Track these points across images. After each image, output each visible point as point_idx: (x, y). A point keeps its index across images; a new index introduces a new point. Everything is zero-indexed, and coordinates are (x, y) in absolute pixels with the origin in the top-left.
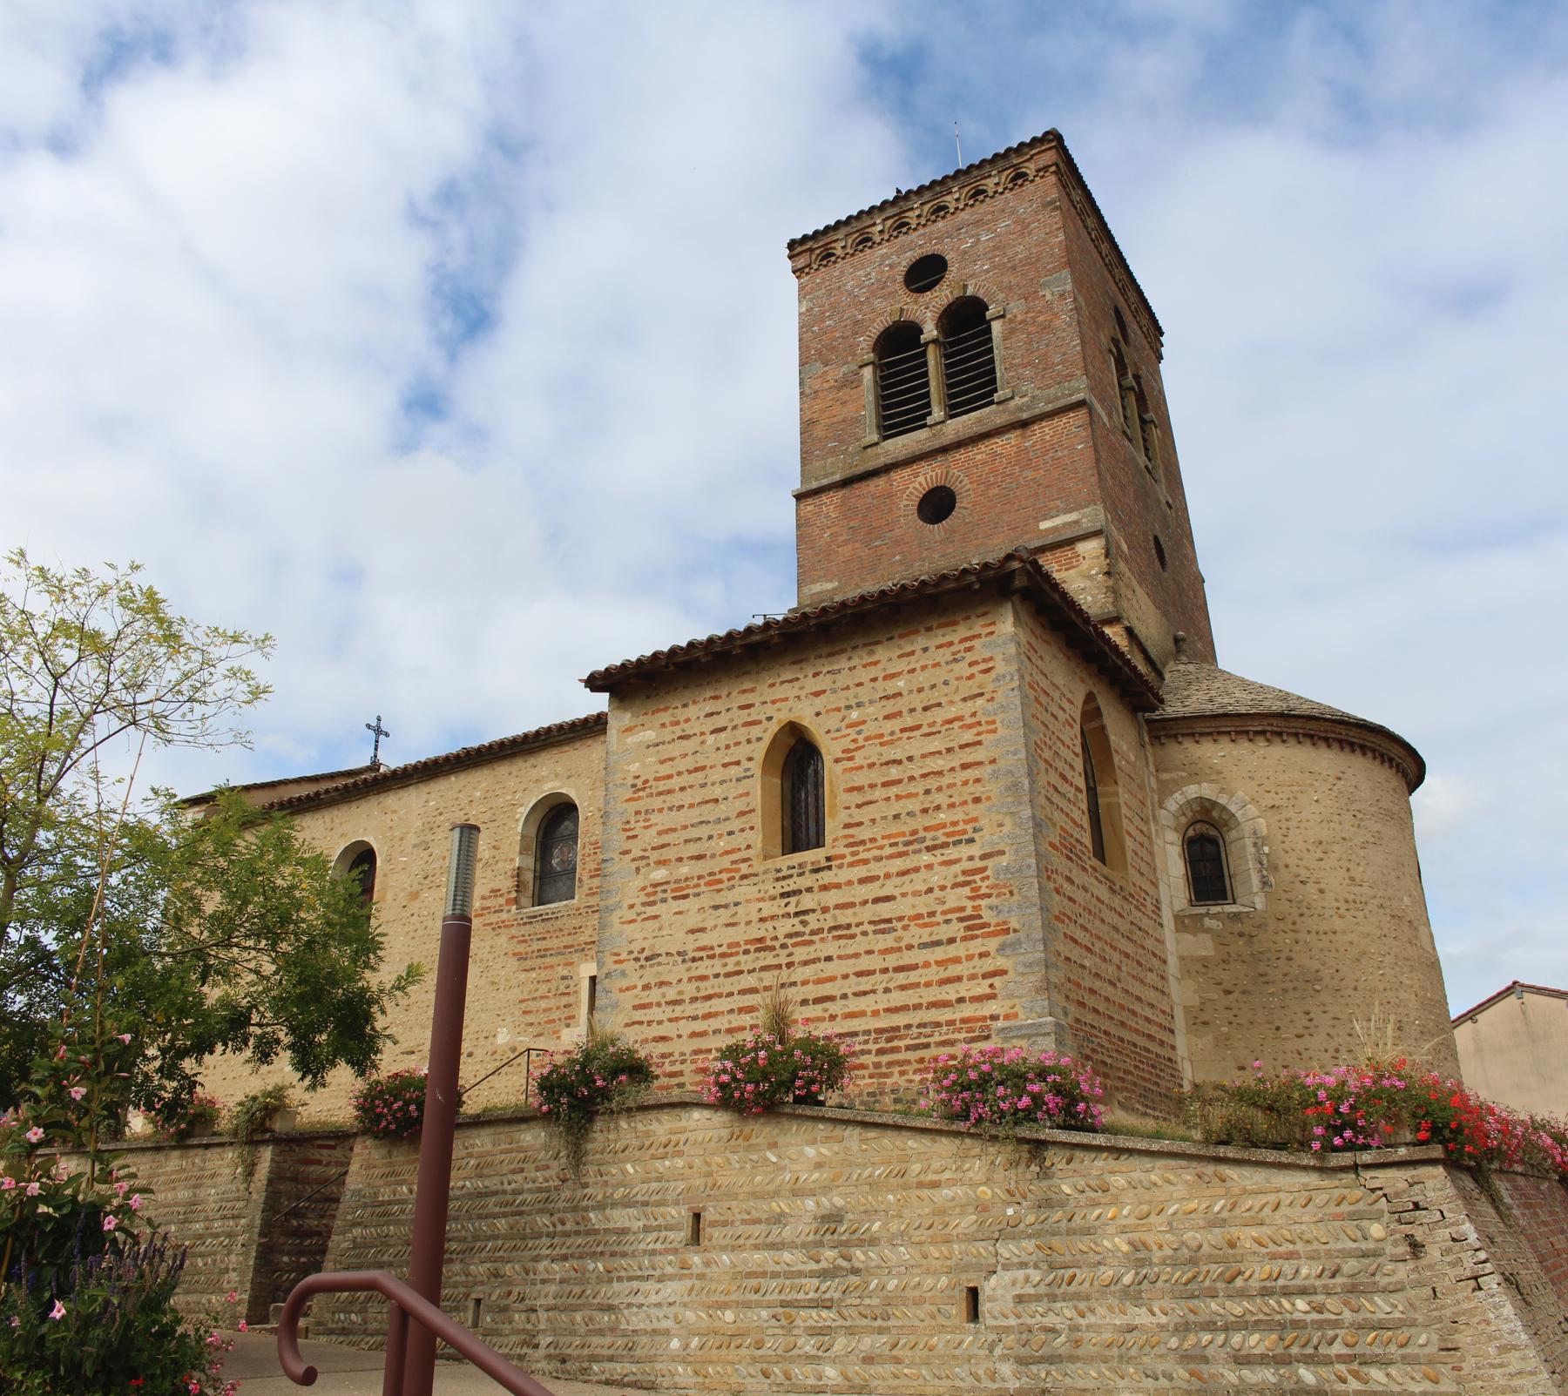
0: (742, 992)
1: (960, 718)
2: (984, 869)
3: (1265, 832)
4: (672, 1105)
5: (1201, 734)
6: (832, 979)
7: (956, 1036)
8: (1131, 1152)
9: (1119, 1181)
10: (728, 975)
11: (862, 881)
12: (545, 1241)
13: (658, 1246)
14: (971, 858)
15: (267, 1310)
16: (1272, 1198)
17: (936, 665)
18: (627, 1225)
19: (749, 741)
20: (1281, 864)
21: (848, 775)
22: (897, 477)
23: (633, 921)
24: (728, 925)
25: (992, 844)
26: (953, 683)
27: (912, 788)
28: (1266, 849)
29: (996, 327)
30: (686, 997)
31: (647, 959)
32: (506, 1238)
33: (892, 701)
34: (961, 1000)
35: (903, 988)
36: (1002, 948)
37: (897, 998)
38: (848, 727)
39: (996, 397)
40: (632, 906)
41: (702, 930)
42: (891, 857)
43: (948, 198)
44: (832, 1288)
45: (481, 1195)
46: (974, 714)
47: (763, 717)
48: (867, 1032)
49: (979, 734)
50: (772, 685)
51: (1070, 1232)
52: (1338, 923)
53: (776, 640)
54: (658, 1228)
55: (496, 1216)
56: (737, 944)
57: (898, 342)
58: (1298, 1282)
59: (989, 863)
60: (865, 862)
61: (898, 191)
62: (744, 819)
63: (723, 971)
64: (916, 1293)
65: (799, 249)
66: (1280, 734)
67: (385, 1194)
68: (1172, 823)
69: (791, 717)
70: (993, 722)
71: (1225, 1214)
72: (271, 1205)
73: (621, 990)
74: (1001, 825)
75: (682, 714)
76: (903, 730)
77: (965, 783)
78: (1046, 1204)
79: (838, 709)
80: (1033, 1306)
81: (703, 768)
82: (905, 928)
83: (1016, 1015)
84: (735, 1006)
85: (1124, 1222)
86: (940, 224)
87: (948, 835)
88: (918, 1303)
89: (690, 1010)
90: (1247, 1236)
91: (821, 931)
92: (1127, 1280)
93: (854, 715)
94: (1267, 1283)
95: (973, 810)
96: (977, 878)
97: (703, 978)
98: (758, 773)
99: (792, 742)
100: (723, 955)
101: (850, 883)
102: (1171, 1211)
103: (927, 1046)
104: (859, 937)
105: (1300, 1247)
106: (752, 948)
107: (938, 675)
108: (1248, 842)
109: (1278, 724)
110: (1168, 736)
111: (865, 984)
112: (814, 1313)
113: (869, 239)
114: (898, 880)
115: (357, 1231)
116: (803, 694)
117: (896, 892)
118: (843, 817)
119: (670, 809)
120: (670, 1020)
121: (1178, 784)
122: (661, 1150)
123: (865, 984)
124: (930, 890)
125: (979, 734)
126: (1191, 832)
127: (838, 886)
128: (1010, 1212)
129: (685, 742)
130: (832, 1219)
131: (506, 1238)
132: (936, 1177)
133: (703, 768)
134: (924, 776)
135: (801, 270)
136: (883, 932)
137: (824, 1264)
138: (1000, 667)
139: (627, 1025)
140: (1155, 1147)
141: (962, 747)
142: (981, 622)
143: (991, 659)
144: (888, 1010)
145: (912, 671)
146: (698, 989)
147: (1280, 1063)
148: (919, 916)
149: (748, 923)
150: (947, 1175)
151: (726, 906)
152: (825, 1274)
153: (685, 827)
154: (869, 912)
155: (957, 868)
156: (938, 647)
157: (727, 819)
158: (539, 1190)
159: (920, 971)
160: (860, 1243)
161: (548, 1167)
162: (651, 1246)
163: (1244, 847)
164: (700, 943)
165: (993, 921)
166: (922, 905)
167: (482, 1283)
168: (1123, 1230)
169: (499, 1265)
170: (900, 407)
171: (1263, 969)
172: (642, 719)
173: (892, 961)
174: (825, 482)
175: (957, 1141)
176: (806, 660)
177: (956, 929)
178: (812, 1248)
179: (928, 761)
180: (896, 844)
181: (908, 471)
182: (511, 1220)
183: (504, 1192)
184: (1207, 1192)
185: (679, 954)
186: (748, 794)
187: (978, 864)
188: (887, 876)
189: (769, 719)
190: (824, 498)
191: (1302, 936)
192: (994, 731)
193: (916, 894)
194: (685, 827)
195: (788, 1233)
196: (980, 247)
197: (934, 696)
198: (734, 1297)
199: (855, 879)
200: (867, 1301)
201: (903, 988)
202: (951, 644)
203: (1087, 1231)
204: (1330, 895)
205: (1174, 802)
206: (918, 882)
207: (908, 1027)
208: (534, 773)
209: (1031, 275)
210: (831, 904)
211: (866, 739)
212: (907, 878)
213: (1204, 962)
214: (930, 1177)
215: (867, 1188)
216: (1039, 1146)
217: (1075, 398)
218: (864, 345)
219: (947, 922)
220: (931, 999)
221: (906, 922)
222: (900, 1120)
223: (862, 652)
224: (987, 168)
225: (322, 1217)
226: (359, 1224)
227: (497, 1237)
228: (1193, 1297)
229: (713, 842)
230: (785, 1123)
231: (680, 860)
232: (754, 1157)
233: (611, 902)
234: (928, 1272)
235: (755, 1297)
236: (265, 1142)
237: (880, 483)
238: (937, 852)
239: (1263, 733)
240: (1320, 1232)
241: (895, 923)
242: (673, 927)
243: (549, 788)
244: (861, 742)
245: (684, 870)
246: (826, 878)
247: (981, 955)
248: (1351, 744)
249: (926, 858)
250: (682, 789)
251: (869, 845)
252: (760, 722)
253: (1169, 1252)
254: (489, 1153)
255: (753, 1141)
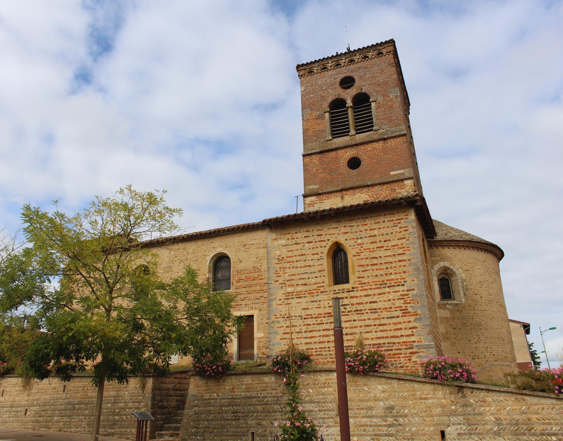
0: (324, 330)
1: (397, 245)
2: (408, 295)
3: (464, 278)
4: (326, 371)
5: (445, 246)
6: (356, 327)
7: (401, 347)
8: (493, 391)
9: (489, 399)
10: (318, 324)
11: (365, 296)
12: (278, 413)
13: (325, 416)
14: (403, 291)
15: (155, 434)
16: (541, 406)
17: (388, 227)
18: (312, 409)
19: (321, 247)
20: (469, 288)
21: (358, 261)
22: (340, 152)
23: (281, 304)
24: (317, 308)
25: (410, 286)
26: (394, 234)
27: (381, 267)
28: (465, 284)
29: (373, 105)
30: (303, 331)
31: (287, 317)
32: (262, 412)
33: (373, 238)
34: (402, 336)
35: (382, 331)
36: (415, 320)
37: (380, 334)
38: (357, 245)
39: (374, 128)
40: (280, 300)
41: (308, 309)
42: (375, 289)
43: (355, 57)
44: (392, 430)
45: (249, 398)
46: (402, 244)
47: (326, 239)
48: (370, 345)
49: (404, 251)
50: (329, 229)
51: (474, 414)
52: (486, 308)
53: (333, 215)
54: (325, 410)
55: (256, 405)
56: (321, 314)
57: (337, 105)
58: (552, 432)
59: (410, 293)
60: (366, 290)
61: (337, 53)
62: (321, 273)
63: (316, 323)
64: (423, 432)
65: (301, 68)
66: (468, 247)
67: (207, 396)
68: (435, 274)
69: (337, 240)
70: (409, 247)
71: (526, 411)
72: (153, 399)
73: (278, 328)
74: (413, 281)
75: (295, 236)
76: (377, 248)
77: (400, 266)
78: (465, 405)
79: (354, 239)
80: (464, 437)
81: (304, 255)
82: (381, 312)
83: (421, 341)
84: (321, 334)
85: (492, 412)
86: (352, 66)
87: (395, 283)
88: (424, 435)
89: (305, 335)
90: (534, 417)
91: (351, 311)
92: (495, 429)
93: (360, 241)
94: (543, 432)
95: (403, 275)
96: (406, 297)
97: (309, 325)
98: (325, 258)
99: (335, 248)
100: (316, 318)
101: (361, 296)
102: (508, 409)
103: (392, 350)
104: (365, 314)
105: (552, 421)
106: (327, 316)
107: (389, 230)
108: (460, 281)
109: (468, 243)
110: (434, 246)
111: (368, 329)
112: (387, 438)
113: (326, 68)
114: (378, 296)
115: (196, 409)
116: (340, 232)
117: (378, 300)
118: (357, 274)
119: (293, 268)
120: (297, 338)
121: (438, 262)
122: (323, 385)
123: (368, 329)
124: (390, 300)
125: (404, 251)
126: (440, 277)
127: (357, 297)
128: (453, 407)
129: (297, 245)
130: (391, 408)
131: (262, 412)
132: (426, 396)
133: (304, 255)
134: (386, 263)
135: (302, 76)
136: (373, 313)
137: (388, 423)
138: (410, 230)
139: (281, 339)
140: (502, 390)
141: (398, 255)
142: (403, 214)
143: (407, 227)
144: (376, 338)
145: (380, 228)
146: (307, 328)
147: (470, 351)
148: (386, 308)
149: (325, 307)
150: (430, 396)
151: (316, 301)
152: (389, 426)
153: (299, 274)
154: (368, 306)
155: (399, 294)
156: (388, 221)
157: (315, 272)
158: (274, 397)
159: (387, 326)
160: (401, 416)
161: (276, 389)
162: (322, 416)
163: (458, 282)
164: (307, 313)
165: (412, 311)
166: (387, 305)
167: (254, 427)
168: (492, 414)
169: (260, 421)
170: (339, 129)
171: (465, 322)
172: (280, 236)
173: (377, 322)
174: (314, 151)
175: (433, 385)
176: (341, 221)
177: (399, 313)
178: (384, 417)
179: (387, 258)
180: (377, 285)
181: (343, 151)
182: (263, 406)
183: (259, 397)
184: (520, 404)
185: (299, 316)
186: (322, 265)
187: (406, 293)
188: (374, 295)
189: (328, 240)
190: (313, 157)
191: (476, 311)
192: (410, 250)
193: (384, 301)
194: (299, 274)
195: (374, 412)
196: (367, 76)
197: (388, 237)
198: (356, 433)
199: (363, 295)
200: (406, 434)
201: (382, 331)
202: (393, 221)
203: (480, 414)
204: (483, 299)
205: (437, 267)
206: (385, 297)
207: (384, 343)
208: (213, 245)
209: (385, 88)
210: (354, 303)
211: (364, 249)
212: (381, 296)
213: (447, 319)
214: (424, 396)
215: (402, 399)
216: (462, 387)
217: (403, 133)
218: (326, 105)
219: (396, 311)
220: (392, 335)
221: (381, 310)
222: (412, 378)
223: (362, 220)
224: (369, 49)
225: (168, 401)
226: (197, 406)
227: (258, 412)
228: (518, 435)
229: (310, 280)
230: (370, 378)
231: (298, 285)
232: (359, 388)
233: (272, 297)
234: (426, 425)
235: (364, 433)
236: (150, 377)
237: (334, 153)
238: (392, 288)
239: (463, 246)
240: (558, 417)
241: (378, 310)
242: (297, 307)
243: (219, 250)
244: (362, 251)
245: (300, 288)
246: (352, 294)
247: (408, 322)
248: (488, 250)
249: (387, 290)
250: (297, 261)
251: (367, 284)
252: (325, 241)
253: (508, 421)
254: (250, 384)
255: (358, 383)
